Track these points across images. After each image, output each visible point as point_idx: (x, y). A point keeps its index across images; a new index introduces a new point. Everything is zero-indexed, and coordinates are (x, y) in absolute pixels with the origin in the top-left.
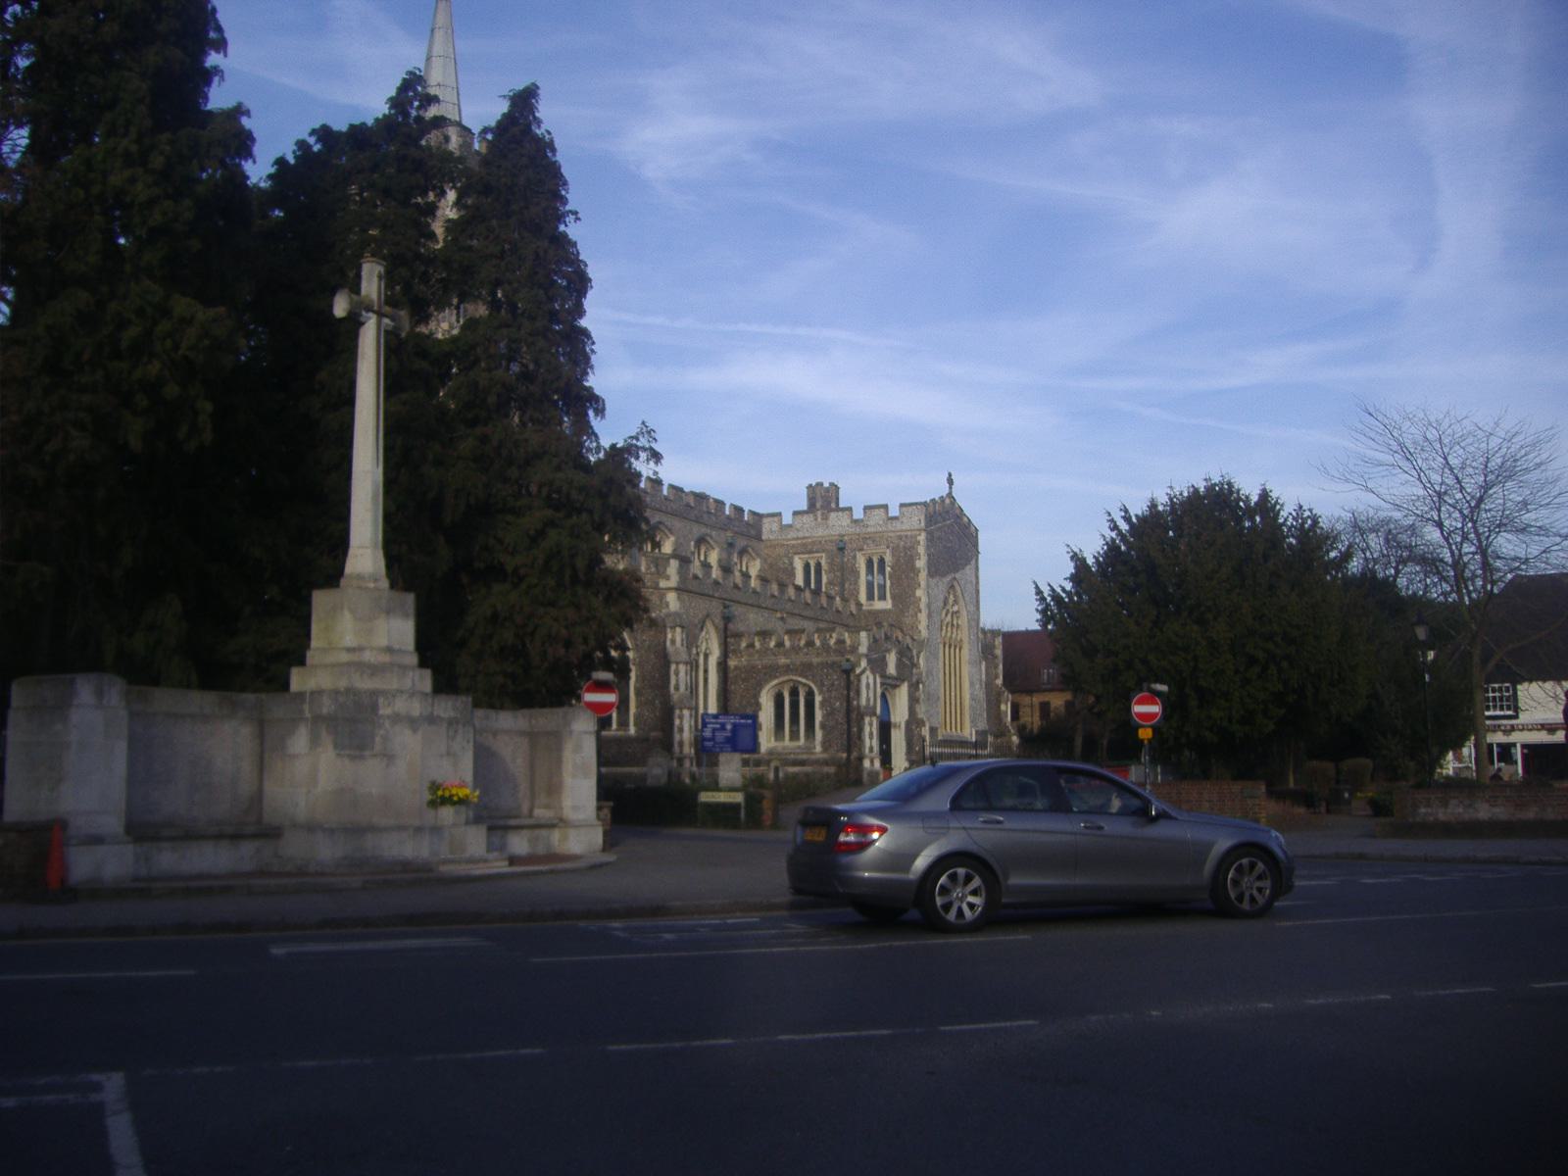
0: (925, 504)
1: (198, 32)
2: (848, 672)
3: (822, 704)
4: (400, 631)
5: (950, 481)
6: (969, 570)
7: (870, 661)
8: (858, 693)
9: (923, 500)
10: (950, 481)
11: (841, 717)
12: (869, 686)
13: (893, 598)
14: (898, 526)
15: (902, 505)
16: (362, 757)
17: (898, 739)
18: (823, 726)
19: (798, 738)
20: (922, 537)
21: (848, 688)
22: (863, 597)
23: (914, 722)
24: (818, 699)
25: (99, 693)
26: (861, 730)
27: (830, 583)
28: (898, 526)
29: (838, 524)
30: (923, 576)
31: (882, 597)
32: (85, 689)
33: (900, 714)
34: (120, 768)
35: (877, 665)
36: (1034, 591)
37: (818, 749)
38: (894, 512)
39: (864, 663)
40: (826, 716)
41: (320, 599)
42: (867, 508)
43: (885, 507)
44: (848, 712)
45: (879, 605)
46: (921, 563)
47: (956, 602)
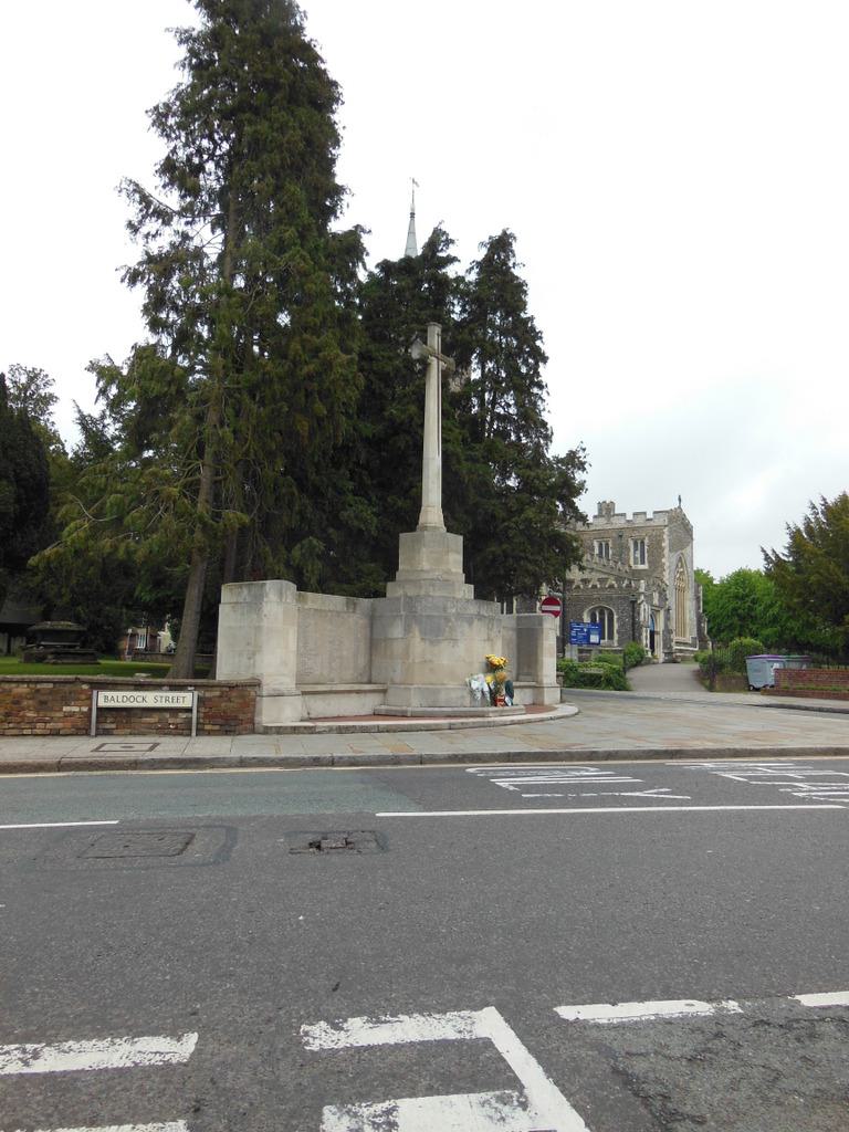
0: (667, 512)
1: (290, 11)
2: (633, 602)
3: (618, 619)
4: (455, 562)
5: (680, 500)
6: (688, 549)
7: (645, 596)
8: (639, 614)
9: (668, 509)
10: (680, 500)
11: (629, 627)
12: (644, 611)
13: (649, 562)
14: (652, 523)
15: (655, 512)
16: (439, 642)
17: (659, 639)
18: (618, 632)
19: (512, 612)
20: (666, 530)
21: (633, 612)
22: (632, 563)
23: (668, 631)
24: (615, 617)
25: (281, 594)
26: (641, 634)
27: (613, 554)
28: (652, 523)
29: (618, 523)
30: (666, 551)
31: (643, 563)
32: (269, 583)
33: (660, 627)
34: (293, 646)
35: (649, 598)
36: (762, 556)
37: (616, 644)
38: (650, 516)
39: (642, 597)
40: (621, 626)
41: (405, 538)
42: (635, 514)
43: (645, 513)
44: (633, 624)
45: (641, 567)
46: (665, 544)
47: (682, 566)
